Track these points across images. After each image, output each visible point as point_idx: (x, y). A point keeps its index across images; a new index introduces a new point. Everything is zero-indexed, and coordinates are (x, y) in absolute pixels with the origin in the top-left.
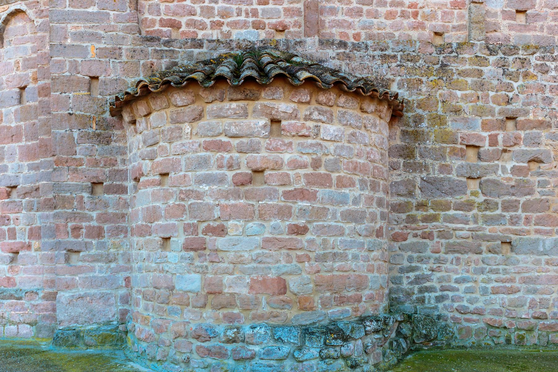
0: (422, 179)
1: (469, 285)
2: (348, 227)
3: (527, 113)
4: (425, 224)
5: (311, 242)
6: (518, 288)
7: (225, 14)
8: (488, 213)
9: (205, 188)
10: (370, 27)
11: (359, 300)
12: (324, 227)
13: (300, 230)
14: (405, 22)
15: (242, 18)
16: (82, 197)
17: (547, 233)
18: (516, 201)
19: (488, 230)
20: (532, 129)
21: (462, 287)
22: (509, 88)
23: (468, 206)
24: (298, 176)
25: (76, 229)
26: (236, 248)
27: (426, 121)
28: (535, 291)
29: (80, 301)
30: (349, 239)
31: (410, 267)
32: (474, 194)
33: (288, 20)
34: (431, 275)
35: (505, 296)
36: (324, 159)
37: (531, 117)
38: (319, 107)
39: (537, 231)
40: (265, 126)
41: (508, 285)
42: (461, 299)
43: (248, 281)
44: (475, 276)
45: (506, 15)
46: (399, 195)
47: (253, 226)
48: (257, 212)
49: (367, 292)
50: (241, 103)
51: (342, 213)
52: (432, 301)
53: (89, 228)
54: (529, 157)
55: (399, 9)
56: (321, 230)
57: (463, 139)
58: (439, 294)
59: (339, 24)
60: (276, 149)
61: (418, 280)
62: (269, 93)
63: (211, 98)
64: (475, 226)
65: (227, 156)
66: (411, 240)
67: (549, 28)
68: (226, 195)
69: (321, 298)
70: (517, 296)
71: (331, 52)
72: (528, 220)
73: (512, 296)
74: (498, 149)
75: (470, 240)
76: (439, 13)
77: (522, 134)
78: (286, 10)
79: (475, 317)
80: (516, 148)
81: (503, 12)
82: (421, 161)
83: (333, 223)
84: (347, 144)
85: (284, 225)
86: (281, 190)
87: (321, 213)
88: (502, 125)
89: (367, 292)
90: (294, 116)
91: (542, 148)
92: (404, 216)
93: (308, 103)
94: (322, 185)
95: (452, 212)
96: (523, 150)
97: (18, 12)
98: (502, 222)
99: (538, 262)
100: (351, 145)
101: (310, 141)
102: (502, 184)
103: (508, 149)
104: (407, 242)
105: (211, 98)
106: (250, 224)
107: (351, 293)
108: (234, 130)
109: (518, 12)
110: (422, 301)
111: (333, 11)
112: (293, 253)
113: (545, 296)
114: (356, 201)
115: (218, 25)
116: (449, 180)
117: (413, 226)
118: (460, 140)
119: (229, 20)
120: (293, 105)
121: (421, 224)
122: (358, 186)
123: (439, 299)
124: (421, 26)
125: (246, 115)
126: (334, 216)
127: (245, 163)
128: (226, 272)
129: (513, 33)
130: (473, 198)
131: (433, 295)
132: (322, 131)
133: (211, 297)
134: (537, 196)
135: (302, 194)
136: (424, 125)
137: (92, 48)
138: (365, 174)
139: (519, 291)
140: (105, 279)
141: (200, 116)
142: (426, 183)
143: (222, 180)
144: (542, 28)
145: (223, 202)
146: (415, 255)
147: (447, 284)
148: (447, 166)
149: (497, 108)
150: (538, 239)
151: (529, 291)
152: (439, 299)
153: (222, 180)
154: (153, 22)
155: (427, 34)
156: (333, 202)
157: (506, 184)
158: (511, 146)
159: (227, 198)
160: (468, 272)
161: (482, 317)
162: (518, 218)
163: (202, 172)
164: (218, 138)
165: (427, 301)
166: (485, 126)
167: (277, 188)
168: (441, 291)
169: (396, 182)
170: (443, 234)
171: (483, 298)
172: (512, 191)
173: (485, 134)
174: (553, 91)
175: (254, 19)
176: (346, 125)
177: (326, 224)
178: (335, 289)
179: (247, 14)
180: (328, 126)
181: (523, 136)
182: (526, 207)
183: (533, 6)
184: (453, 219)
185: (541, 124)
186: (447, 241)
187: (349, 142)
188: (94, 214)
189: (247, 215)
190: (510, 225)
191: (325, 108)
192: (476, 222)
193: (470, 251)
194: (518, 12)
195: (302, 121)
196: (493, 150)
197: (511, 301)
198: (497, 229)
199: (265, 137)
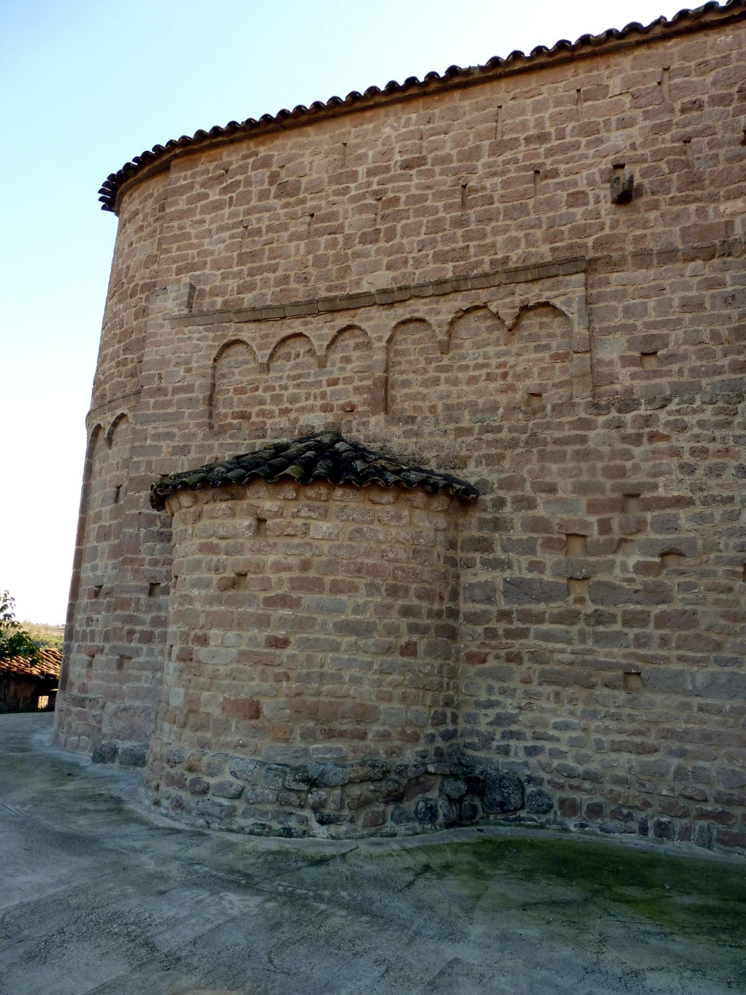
0: (505, 580)
1: (574, 734)
2: (346, 640)
3: (655, 487)
4: (509, 641)
5: (292, 657)
6: (654, 746)
7: (294, 399)
8: (601, 628)
9: (196, 592)
10: (448, 396)
11: (363, 736)
12: (308, 640)
13: (281, 643)
14: (492, 386)
15: (310, 402)
16: (139, 599)
17: (696, 661)
18: (643, 611)
19: (602, 654)
20: (664, 508)
21: (566, 736)
22: (627, 455)
23: (572, 617)
24: (280, 581)
25: (131, 633)
26: (214, 661)
27: (509, 505)
28: (682, 753)
29: (124, 714)
30: (346, 657)
31: (489, 700)
32: (580, 600)
33: (355, 399)
34: (518, 715)
35: (633, 757)
36: (316, 560)
37: (661, 492)
38: (310, 503)
39: (681, 659)
40: (250, 526)
41: (638, 739)
42: (562, 754)
43: (221, 699)
44: (584, 722)
45: (626, 361)
46: (474, 601)
47: (231, 635)
48: (236, 621)
49: (376, 728)
50: (230, 503)
51: (336, 625)
52: (522, 753)
53: (142, 633)
54: (659, 549)
55: (484, 372)
56: (305, 644)
57: (561, 526)
58: (530, 744)
59: (413, 397)
60: (259, 551)
61: (499, 720)
62: (254, 491)
63: (206, 499)
64: (581, 647)
65: (215, 558)
66: (491, 663)
67: (692, 370)
68: (210, 601)
69: (301, 728)
70: (652, 758)
71: (398, 430)
72: (664, 641)
73: (645, 758)
74: (612, 539)
75: (577, 669)
76: (536, 371)
77: (649, 516)
78: (356, 389)
79: (587, 785)
80: (641, 537)
81: (622, 358)
82: (503, 557)
83: (322, 636)
84: (347, 542)
85: (262, 635)
86: (263, 595)
87: (304, 624)
88: (620, 506)
89: (376, 728)
90: (279, 514)
91: (683, 536)
92: (480, 629)
93: (296, 499)
94: (310, 590)
95: (546, 627)
96: (651, 540)
97: (122, 416)
98: (622, 642)
99: (686, 706)
100: (353, 544)
101: (296, 541)
102: (621, 588)
103: (629, 538)
104: (487, 665)
105: (206, 499)
106: (229, 634)
107: (345, 726)
108: (221, 532)
109: (644, 354)
110: (505, 751)
111: (406, 384)
112: (270, 671)
113: (701, 763)
114: (357, 610)
115: (285, 412)
116: (541, 582)
117: (494, 643)
118: (556, 528)
119: (297, 405)
120: (278, 503)
121: (504, 641)
122: (364, 591)
123: (531, 751)
124: (512, 388)
125: (233, 515)
126: (323, 626)
127: (232, 564)
128: (203, 688)
129: (636, 382)
130: (578, 607)
131: (522, 744)
132: (312, 528)
133: (191, 715)
134: (680, 607)
135: (283, 601)
136: (508, 508)
137: (166, 446)
138: (375, 577)
139: (656, 750)
140: (150, 690)
141: (199, 516)
142: (510, 586)
143: (208, 584)
144: (681, 372)
145: (208, 608)
146: (497, 685)
147: (542, 731)
148: (538, 562)
149: (609, 483)
150: (682, 671)
151: (672, 753)
152: (531, 751)
153: (208, 584)
154: (226, 416)
155: (519, 396)
156: (321, 609)
157: (627, 587)
158: (632, 534)
159: (211, 604)
160: (572, 713)
161: (598, 786)
162: (649, 637)
163: (196, 575)
164: (210, 540)
165: (512, 753)
166: (592, 508)
167: (257, 594)
168: (533, 738)
169: (470, 585)
170: (536, 657)
171: (598, 757)
172: (635, 597)
173: (593, 519)
174: (696, 454)
175: (323, 402)
176: (348, 520)
177: (311, 636)
178: (322, 720)
179: (315, 398)
180: (320, 523)
181: (649, 520)
182: (662, 621)
183: (666, 345)
184: (548, 637)
185: (680, 502)
186: (542, 666)
187: (350, 539)
188: (148, 617)
189: (225, 622)
190: (636, 647)
191: (317, 504)
192: (583, 641)
193: (575, 683)
194: (644, 354)
195: (290, 519)
196: (605, 541)
197: (643, 765)
198: (617, 654)
199: (249, 538)
